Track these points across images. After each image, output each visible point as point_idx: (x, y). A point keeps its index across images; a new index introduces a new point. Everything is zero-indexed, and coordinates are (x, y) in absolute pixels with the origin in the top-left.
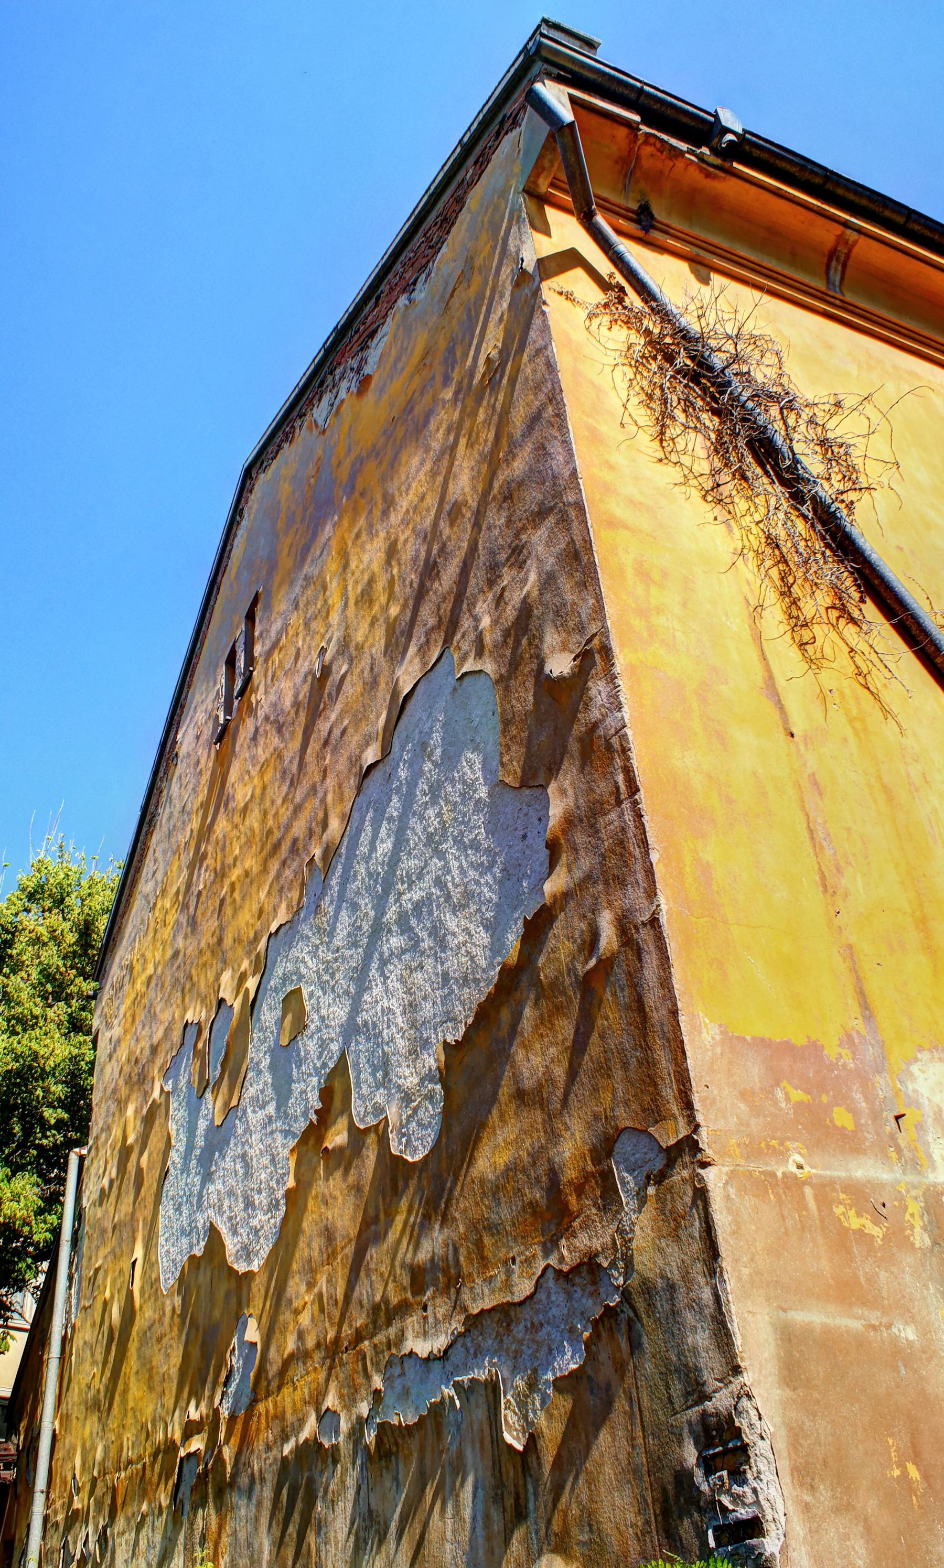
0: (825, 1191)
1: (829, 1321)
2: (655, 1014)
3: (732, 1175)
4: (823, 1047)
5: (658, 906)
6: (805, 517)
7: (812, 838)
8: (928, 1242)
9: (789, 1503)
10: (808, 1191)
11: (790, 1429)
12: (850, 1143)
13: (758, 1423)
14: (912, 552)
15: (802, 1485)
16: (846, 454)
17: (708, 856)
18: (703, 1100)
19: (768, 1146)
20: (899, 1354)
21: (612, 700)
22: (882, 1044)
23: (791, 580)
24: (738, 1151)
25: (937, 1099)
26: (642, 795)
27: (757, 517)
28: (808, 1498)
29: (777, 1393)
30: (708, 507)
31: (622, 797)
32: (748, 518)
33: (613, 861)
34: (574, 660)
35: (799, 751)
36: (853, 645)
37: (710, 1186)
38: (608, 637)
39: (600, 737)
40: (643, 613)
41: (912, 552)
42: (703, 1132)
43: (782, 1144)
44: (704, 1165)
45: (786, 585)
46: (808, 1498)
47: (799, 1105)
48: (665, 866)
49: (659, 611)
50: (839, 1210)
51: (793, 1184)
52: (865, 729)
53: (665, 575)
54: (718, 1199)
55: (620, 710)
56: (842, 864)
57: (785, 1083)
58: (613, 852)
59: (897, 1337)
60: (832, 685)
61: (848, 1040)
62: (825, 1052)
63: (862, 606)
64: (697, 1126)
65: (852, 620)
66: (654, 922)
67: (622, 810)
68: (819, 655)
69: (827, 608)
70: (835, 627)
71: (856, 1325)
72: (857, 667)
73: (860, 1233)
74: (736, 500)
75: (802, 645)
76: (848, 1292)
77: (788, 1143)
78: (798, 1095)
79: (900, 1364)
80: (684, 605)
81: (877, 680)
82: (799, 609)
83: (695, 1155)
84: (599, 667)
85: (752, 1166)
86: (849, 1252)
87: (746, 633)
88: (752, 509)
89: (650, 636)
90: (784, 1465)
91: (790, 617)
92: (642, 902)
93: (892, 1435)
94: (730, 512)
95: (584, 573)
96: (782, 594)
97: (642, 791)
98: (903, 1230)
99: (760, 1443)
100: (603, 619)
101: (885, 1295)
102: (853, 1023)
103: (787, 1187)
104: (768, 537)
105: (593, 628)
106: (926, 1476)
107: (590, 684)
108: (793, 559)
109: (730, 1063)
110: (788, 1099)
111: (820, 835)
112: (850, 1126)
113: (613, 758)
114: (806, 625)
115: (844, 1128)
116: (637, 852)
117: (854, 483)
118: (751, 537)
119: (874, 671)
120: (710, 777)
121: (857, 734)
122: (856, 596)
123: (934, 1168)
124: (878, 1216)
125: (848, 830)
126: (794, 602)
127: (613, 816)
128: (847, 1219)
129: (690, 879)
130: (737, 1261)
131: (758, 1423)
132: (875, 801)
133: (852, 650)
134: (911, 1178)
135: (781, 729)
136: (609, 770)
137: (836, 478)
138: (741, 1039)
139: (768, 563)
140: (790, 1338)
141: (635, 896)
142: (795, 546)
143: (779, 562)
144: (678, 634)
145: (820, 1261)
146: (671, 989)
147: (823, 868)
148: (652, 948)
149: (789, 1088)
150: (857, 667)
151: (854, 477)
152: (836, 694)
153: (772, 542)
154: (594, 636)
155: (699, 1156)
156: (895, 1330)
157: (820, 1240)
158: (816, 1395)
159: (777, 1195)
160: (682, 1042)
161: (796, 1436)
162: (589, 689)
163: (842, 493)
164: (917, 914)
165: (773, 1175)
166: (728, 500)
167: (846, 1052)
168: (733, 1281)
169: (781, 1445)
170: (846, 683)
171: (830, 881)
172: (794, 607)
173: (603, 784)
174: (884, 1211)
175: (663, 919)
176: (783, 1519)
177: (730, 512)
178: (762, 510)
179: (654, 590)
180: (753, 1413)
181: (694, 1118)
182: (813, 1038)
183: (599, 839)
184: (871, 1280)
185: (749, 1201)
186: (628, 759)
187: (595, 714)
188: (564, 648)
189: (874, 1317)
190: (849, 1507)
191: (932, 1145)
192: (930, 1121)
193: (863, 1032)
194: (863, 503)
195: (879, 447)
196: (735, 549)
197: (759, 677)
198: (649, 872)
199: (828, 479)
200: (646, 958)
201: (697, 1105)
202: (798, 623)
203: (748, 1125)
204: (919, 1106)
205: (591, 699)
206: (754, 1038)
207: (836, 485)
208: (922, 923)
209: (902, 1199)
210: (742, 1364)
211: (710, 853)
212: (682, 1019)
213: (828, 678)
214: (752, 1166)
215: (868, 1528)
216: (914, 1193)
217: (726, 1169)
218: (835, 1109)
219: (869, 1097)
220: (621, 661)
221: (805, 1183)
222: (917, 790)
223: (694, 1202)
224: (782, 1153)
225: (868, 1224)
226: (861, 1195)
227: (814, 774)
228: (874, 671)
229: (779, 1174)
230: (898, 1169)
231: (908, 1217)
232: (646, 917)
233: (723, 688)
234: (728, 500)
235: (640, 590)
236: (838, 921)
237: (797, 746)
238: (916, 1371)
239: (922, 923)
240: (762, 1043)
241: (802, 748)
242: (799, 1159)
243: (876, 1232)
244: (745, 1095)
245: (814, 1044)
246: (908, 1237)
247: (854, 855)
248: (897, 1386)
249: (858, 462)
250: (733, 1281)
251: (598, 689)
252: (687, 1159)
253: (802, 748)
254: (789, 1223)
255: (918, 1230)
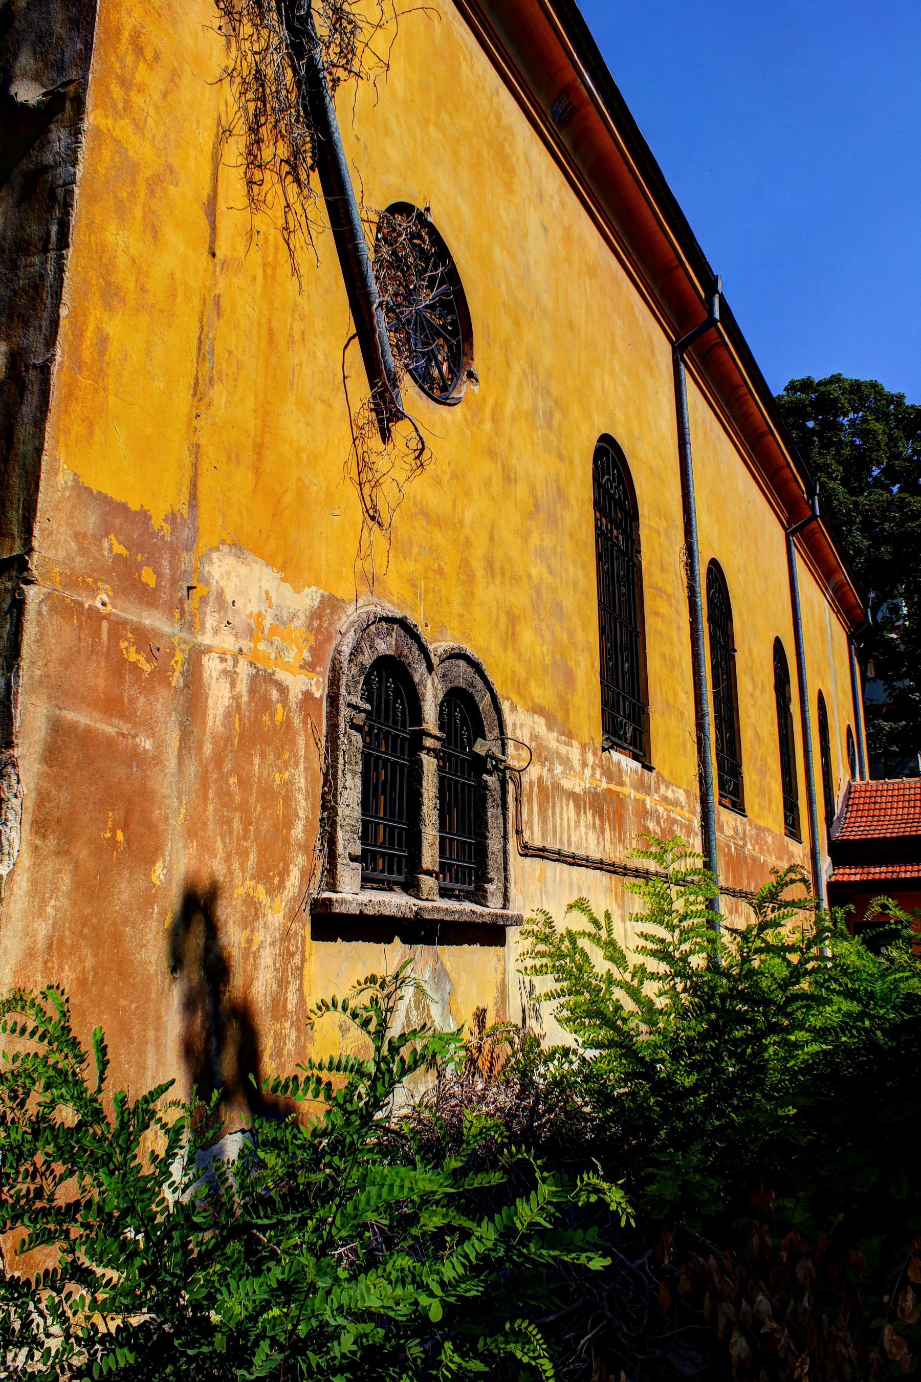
0: (118, 626)
1: (92, 724)
2: (21, 446)
3: (48, 596)
4: (151, 518)
5: (54, 355)
6: (295, 71)
7: (199, 349)
8: (182, 684)
9: (24, 844)
10: (105, 624)
11: (39, 794)
12: (148, 597)
13: (15, 786)
14: (366, 146)
15: (37, 833)
16: (352, 33)
17: (110, 330)
18: (42, 530)
19: (84, 581)
20: (136, 757)
21: (69, 152)
22: (196, 530)
23: (263, 120)
24: (58, 579)
25: (222, 583)
26: (70, 252)
27: (256, 48)
28: (39, 842)
29: (36, 767)
30: (218, 13)
31: (51, 247)
32: (248, 44)
33: (22, 301)
34: (44, 95)
35: (215, 271)
36: (291, 201)
37: (29, 600)
38: (85, 90)
39: (46, 181)
40: (126, 84)
41: (366, 146)
42: (35, 556)
43: (95, 582)
44: (29, 582)
45: (257, 123)
46: (39, 842)
47: (118, 557)
48: (70, 322)
49: (141, 89)
50: (123, 644)
51: (95, 616)
52: (274, 276)
53: (157, 57)
54: (32, 612)
55: (74, 166)
56: (216, 378)
57: (112, 536)
58: (26, 292)
59: (138, 745)
60: (262, 228)
61: (172, 518)
62: (152, 522)
63: (311, 172)
64: (30, 550)
65: (297, 181)
66: (45, 370)
67: (47, 258)
68: (261, 198)
69: (282, 161)
70: (282, 180)
71: (110, 730)
72: (287, 223)
73: (135, 665)
74: (245, 20)
75: (250, 183)
76: (112, 706)
77: (99, 584)
78: (119, 549)
79: (134, 764)
80: (165, 95)
81: (298, 240)
82: (260, 149)
83: (21, 573)
84: (67, 115)
85: (67, 594)
86: (122, 677)
87: (209, 149)
88: (255, 37)
89: (124, 109)
90: (28, 818)
91: (250, 153)
92: (41, 348)
93: (113, 810)
94: (234, 29)
95: (80, 12)
96: (251, 129)
97: (71, 249)
98: (166, 671)
99: (13, 800)
100: (86, 70)
101: (139, 714)
102: (179, 506)
103: (89, 617)
104: (258, 71)
105: (73, 74)
106: (127, 840)
107: (52, 126)
108: (272, 103)
109: (73, 507)
110: (111, 550)
111: (206, 348)
112: (152, 584)
113: (53, 208)
114: (260, 167)
115: (147, 584)
116: (48, 302)
117: (347, 63)
118: (244, 64)
119: (299, 232)
120: (134, 262)
121: (265, 278)
122: (310, 162)
123: (203, 633)
124: (151, 656)
125: (230, 352)
126: (259, 141)
127: (36, 260)
128: (128, 652)
129: (88, 343)
130: (33, 663)
131: (15, 786)
132: (259, 337)
133: (288, 206)
134: (184, 635)
135: (207, 246)
136: (46, 216)
137: (334, 49)
138: (89, 491)
139: (250, 95)
140: (58, 729)
141: (35, 340)
142: (278, 92)
143: (258, 99)
144: (149, 120)
145: (97, 678)
146: (42, 431)
147: (200, 375)
148: (36, 389)
149: (114, 541)
150: (287, 223)
151: (350, 56)
152: (261, 237)
153: (259, 77)
154: (71, 82)
155: (25, 574)
156: (138, 740)
157: (103, 663)
158: (66, 774)
159: (79, 621)
160: (39, 477)
161: (42, 799)
162: (50, 131)
163: (334, 66)
164: (258, 440)
165: (81, 604)
166: (237, 17)
167: (167, 528)
168: (26, 677)
169: (29, 804)
170: (273, 231)
171: (201, 388)
172: (256, 146)
173: (35, 227)
174: (157, 654)
175: (55, 369)
176: (16, 854)
177: (234, 29)
178: (263, 43)
179: (142, 67)
180: (14, 777)
181: (31, 542)
182: (146, 508)
183: (16, 275)
184: (132, 701)
185: (57, 620)
186: (68, 214)
187: (49, 158)
188: (37, 78)
189: (126, 728)
190: (68, 852)
191: (208, 616)
192: (212, 598)
193: (186, 516)
194: (348, 85)
195: (380, 43)
196: (227, 67)
197: (206, 192)
198: (55, 323)
199: (328, 48)
200: (28, 396)
201: (36, 532)
202: (253, 160)
203: (73, 560)
204: (207, 583)
205: (49, 142)
206: (99, 493)
207: (333, 56)
208: (259, 448)
209: (173, 648)
210: (15, 741)
211: (115, 327)
212: (45, 458)
213: (261, 222)
214: (67, 594)
215: (76, 868)
216: (183, 646)
217: (44, 590)
218: (145, 568)
219: (174, 567)
220: (92, 119)
221: (105, 617)
222: (293, 342)
223: (10, 611)
224: (93, 591)
225: (143, 660)
226: (144, 638)
227: (219, 296)
228: (299, 232)
229: (86, 606)
230: (177, 626)
231: (173, 662)
232: (39, 361)
233: (171, 188)
234: (237, 17)
235: (130, 60)
236: (196, 423)
237: (215, 267)
238: (143, 771)
239: (259, 448)
240: (104, 500)
241: (218, 269)
242: (105, 598)
243: (147, 668)
244: (78, 536)
245: (145, 512)
246: (168, 677)
247: (227, 375)
248: (127, 779)
249: (359, 47)
250: (26, 677)
251: (59, 137)
252: (14, 573)
253: (218, 269)
254: (83, 644)
255: (177, 674)
